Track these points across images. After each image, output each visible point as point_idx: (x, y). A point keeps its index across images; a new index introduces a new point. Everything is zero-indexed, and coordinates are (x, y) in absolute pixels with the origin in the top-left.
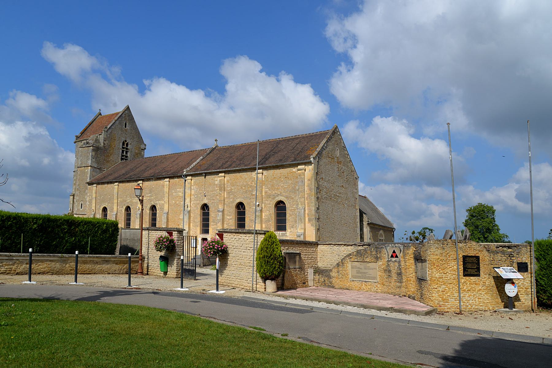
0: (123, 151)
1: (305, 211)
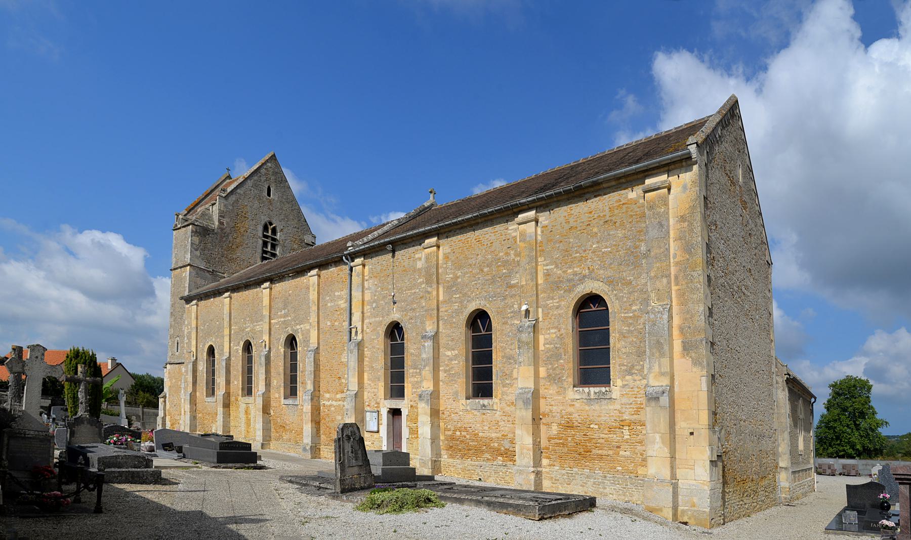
0: (265, 244)
1: (671, 317)
